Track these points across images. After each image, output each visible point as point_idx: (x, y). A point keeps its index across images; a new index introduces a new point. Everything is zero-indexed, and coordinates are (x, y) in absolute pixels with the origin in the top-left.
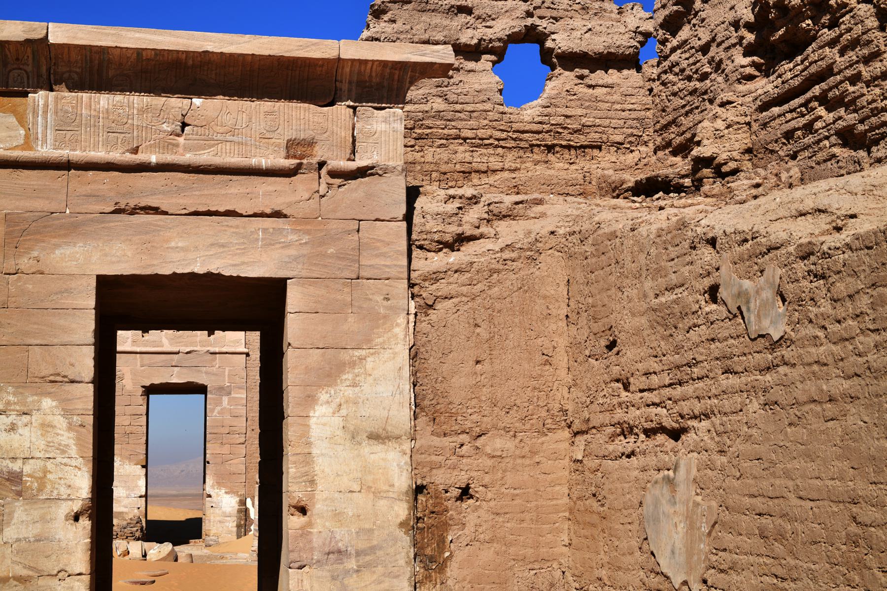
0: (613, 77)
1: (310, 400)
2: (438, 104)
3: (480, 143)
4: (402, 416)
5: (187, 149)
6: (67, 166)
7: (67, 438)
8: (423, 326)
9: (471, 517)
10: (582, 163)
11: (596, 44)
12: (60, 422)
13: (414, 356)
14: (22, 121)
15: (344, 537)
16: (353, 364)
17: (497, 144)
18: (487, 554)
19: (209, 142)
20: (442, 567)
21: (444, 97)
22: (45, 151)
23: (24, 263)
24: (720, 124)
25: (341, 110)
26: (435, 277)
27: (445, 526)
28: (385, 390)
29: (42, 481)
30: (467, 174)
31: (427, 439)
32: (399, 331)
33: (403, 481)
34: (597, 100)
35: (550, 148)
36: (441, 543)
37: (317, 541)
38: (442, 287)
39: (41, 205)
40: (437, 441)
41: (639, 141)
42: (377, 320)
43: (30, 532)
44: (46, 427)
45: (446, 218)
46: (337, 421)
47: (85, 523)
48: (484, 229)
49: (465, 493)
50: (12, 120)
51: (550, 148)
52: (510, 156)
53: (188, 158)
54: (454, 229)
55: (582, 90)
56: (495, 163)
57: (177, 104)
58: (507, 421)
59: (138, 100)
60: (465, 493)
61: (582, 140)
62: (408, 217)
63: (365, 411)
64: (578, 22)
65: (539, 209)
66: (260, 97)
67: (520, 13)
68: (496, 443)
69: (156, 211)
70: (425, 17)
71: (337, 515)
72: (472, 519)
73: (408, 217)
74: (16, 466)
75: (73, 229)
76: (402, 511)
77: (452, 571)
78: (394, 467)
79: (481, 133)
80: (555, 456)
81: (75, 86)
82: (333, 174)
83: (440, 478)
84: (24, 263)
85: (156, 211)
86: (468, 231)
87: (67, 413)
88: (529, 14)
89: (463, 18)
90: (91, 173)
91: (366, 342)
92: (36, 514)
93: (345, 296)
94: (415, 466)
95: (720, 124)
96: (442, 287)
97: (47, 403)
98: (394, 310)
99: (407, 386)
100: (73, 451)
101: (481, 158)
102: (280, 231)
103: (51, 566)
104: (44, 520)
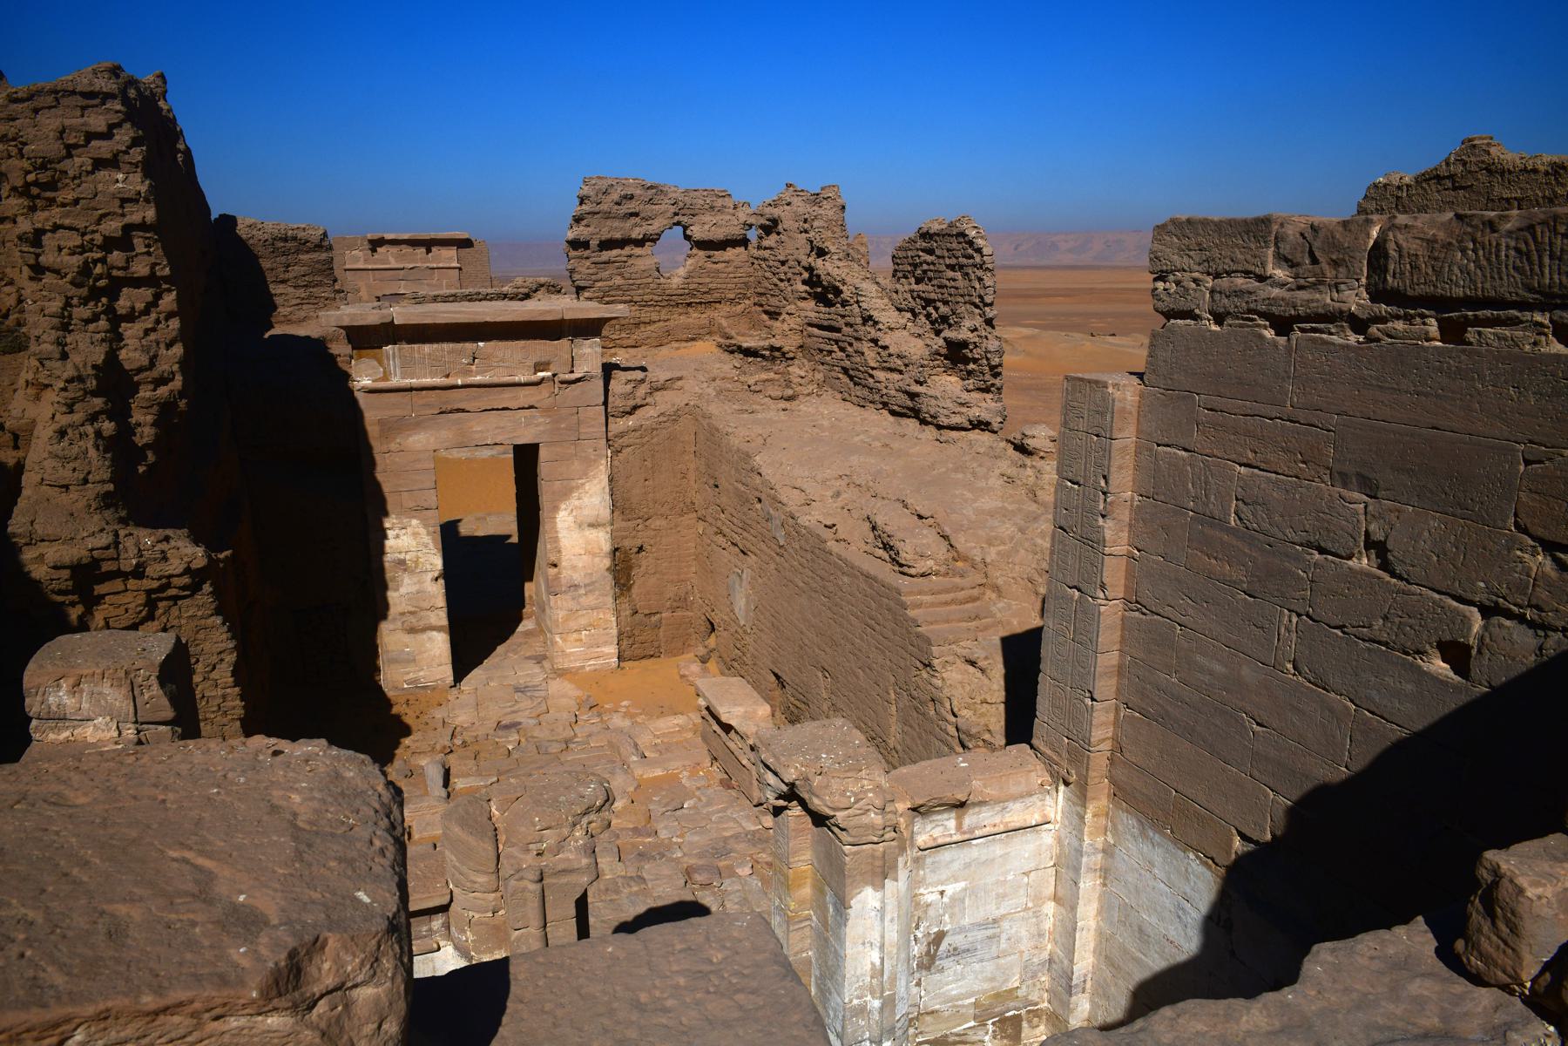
0: (730, 253)
1: (556, 509)
2: (618, 281)
3: (646, 304)
4: (605, 513)
5: (478, 373)
6: (411, 389)
7: (427, 539)
8: (616, 463)
9: (645, 562)
10: (709, 313)
11: (719, 234)
12: (422, 531)
13: (611, 480)
14: (380, 363)
15: (577, 577)
16: (578, 488)
17: (656, 304)
18: (653, 580)
19: (489, 368)
20: (629, 589)
21: (621, 274)
22: (396, 381)
23: (393, 446)
24: (785, 327)
25: (565, 342)
26: (621, 435)
27: (630, 568)
28: (596, 500)
29: (416, 562)
30: (637, 325)
31: (620, 524)
32: (602, 468)
33: (607, 547)
34: (718, 271)
35: (689, 305)
36: (629, 577)
37: (563, 581)
38: (625, 441)
39: (398, 412)
40: (624, 524)
41: (745, 297)
42: (589, 463)
43: (414, 589)
44: (415, 534)
45: (627, 396)
46: (571, 519)
47: (441, 581)
48: (649, 400)
49: (641, 549)
50: (375, 363)
51: (689, 305)
52: (664, 311)
53: (478, 379)
54: (632, 403)
55: (709, 265)
56: (655, 317)
57: (469, 346)
58: (663, 510)
59: (447, 346)
60: (641, 549)
61: (709, 298)
62: (605, 403)
63: (586, 512)
64: (707, 218)
65: (680, 383)
66: (518, 339)
67: (669, 214)
68: (657, 523)
69: (463, 411)
70: (609, 222)
71: (574, 568)
72: (644, 563)
73: (605, 403)
74: (402, 556)
75: (417, 425)
76: (607, 562)
77: (635, 590)
78: (602, 540)
79: (646, 298)
80: (689, 527)
81: (410, 342)
82: (562, 382)
83: (627, 543)
84: (393, 446)
85: (463, 411)
86: (639, 401)
87: (426, 526)
88: (676, 214)
89: (633, 220)
90: (591, 920)
91: (585, 474)
92: (415, 580)
93: (572, 450)
94: (613, 538)
95: (785, 327)
96: (625, 441)
97: (415, 522)
98: (600, 456)
99: (608, 497)
100: (431, 546)
101: (646, 315)
102: (533, 417)
103: (426, 605)
104: (419, 582)
